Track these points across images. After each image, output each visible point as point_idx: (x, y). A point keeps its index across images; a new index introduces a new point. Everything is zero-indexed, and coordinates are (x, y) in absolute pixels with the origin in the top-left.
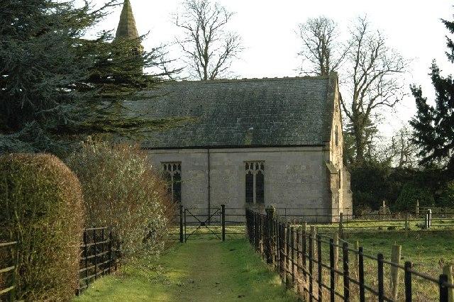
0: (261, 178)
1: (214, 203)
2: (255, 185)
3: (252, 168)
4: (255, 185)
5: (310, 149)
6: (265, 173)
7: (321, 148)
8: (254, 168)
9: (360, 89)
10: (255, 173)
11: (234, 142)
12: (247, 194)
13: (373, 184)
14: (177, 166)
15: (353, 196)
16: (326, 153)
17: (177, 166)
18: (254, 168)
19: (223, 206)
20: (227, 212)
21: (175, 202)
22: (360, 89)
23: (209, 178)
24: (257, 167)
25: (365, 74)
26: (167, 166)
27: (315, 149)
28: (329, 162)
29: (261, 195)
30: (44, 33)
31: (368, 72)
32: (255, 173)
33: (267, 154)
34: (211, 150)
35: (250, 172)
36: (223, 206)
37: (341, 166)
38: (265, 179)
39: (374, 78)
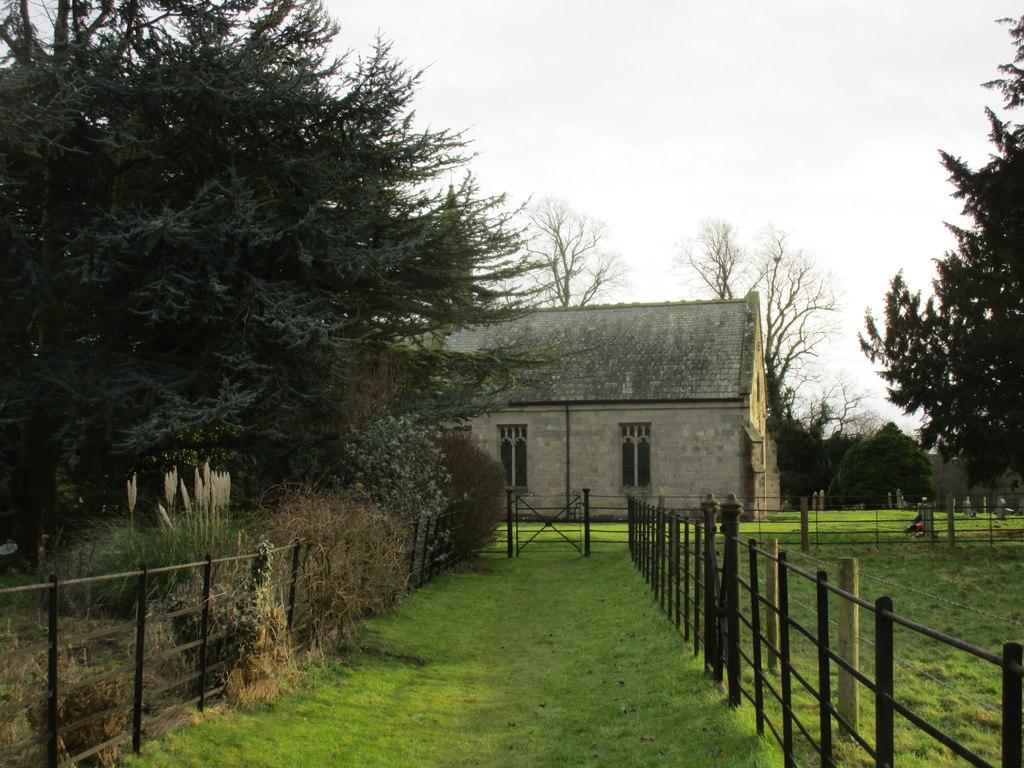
0: (645, 449)
1: (576, 486)
2: (636, 464)
3: (632, 434)
4: (636, 464)
5: (720, 405)
6: (651, 440)
7: (738, 405)
8: (513, 435)
9: (775, 333)
10: (513, 440)
11: (650, 396)
12: (649, 473)
13: (818, 463)
14: (646, 428)
15: (781, 478)
16: (744, 412)
17: (646, 428)
18: (513, 435)
19: (586, 491)
20: (592, 502)
21: (165, 399)
22: (775, 333)
23: (568, 448)
24: (640, 433)
25: (782, 313)
26: (625, 428)
27: (731, 405)
28: (748, 425)
29: (645, 478)
30: (316, 441)
31: (785, 312)
32: (513, 440)
33: (645, 412)
34: (571, 408)
35: (628, 440)
36: (586, 491)
37: (763, 433)
38: (652, 450)
39: (795, 318)
